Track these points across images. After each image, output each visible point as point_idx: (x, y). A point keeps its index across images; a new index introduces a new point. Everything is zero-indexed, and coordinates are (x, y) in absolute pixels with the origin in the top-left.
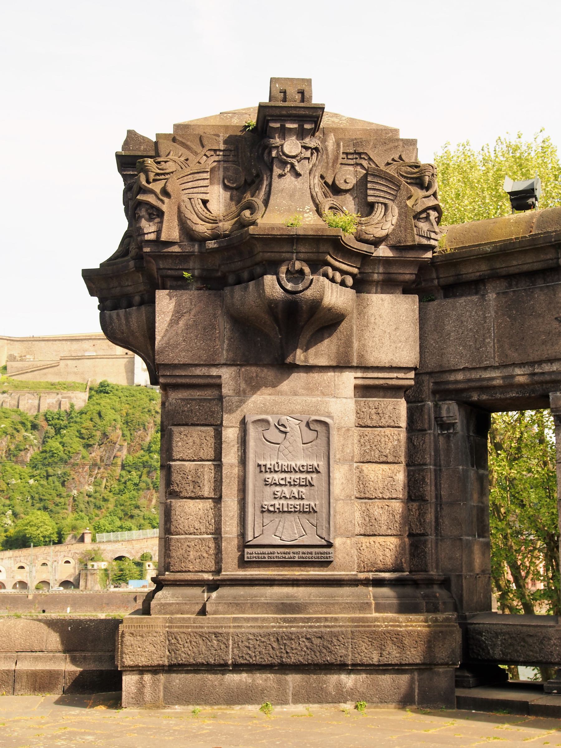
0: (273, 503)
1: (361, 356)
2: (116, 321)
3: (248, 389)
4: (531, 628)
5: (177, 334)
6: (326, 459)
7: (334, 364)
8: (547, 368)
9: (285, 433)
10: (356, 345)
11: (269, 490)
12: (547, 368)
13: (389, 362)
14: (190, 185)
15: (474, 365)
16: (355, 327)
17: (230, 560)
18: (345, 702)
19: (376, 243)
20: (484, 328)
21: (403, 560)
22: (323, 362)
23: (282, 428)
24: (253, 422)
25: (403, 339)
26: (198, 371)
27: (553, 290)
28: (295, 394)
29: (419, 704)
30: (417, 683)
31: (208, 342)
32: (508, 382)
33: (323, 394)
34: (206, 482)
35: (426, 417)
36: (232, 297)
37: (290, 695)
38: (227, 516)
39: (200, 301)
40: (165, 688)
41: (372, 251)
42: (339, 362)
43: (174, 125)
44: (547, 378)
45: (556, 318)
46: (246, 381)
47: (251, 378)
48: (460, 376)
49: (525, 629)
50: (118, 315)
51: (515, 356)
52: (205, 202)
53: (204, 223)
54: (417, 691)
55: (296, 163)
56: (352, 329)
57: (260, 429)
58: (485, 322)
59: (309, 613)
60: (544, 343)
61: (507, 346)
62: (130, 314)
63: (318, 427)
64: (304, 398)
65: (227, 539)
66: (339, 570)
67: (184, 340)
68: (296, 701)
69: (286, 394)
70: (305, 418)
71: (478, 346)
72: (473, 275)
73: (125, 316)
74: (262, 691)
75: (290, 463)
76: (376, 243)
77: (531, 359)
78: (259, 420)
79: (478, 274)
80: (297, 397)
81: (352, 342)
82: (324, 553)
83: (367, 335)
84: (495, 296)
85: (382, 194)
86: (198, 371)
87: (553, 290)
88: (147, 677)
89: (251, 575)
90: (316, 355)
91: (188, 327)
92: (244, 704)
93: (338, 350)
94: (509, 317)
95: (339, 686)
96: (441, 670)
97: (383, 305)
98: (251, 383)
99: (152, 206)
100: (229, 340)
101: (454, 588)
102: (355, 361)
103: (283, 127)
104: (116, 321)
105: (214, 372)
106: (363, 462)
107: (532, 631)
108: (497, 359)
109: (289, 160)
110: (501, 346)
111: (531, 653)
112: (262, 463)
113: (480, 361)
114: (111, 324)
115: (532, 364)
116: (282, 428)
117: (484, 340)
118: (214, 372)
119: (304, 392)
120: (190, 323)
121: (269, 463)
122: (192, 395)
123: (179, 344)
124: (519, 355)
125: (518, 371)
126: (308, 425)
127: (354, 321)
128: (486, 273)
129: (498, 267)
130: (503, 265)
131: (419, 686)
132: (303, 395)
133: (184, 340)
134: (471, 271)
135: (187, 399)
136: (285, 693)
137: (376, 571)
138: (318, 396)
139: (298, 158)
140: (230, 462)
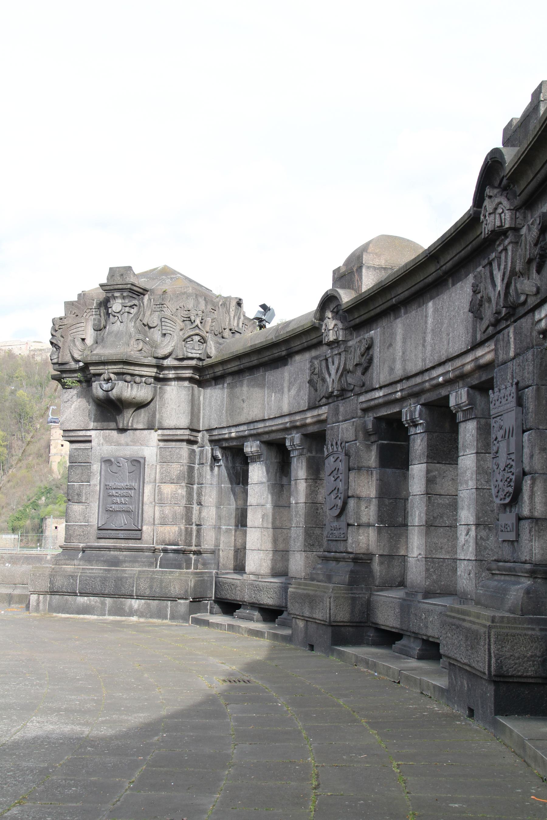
0: (111, 506)
1: (160, 423)
3: (104, 443)
5: (70, 413)
7: (146, 428)
11: (110, 499)
13: (174, 426)
14: (74, 330)
16: (158, 407)
17: (91, 537)
18: (133, 617)
19: (165, 358)
21: (179, 539)
22: (140, 426)
24: (104, 461)
25: (182, 412)
28: (127, 445)
29: (170, 620)
30: (169, 608)
31: (85, 417)
33: (142, 445)
34: (84, 494)
35: (204, 456)
37: (107, 611)
39: (82, 395)
40: (49, 604)
42: (149, 426)
43: (111, 269)
46: (103, 438)
47: (106, 436)
52: (83, 340)
54: (169, 612)
55: (119, 316)
56: (156, 408)
57: (108, 465)
59: (123, 567)
63: (135, 463)
64: (132, 447)
67: (74, 417)
68: (110, 614)
69: (123, 445)
74: (94, 608)
76: (165, 358)
79: (220, 372)
80: (128, 447)
81: (156, 415)
83: (164, 410)
85: (169, 328)
88: (41, 597)
90: (137, 422)
91: (76, 409)
92: (85, 614)
93: (148, 419)
95: (131, 607)
97: (172, 392)
98: (106, 439)
101: (216, 555)
102: (157, 425)
103: (113, 295)
106: (161, 483)
109: (116, 314)
110: (227, 418)
112: (107, 484)
118: (88, 433)
119: (132, 444)
120: (77, 407)
121: (111, 484)
122: (80, 446)
123: (71, 419)
127: (157, 403)
131: (170, 610)
132: (131, 445)
133: (74, 417)
135: (77, 449)
136: (105, 610)
137: (165, 545)
138: (139, 446)
139: (121, 313)
140: (94, 483)
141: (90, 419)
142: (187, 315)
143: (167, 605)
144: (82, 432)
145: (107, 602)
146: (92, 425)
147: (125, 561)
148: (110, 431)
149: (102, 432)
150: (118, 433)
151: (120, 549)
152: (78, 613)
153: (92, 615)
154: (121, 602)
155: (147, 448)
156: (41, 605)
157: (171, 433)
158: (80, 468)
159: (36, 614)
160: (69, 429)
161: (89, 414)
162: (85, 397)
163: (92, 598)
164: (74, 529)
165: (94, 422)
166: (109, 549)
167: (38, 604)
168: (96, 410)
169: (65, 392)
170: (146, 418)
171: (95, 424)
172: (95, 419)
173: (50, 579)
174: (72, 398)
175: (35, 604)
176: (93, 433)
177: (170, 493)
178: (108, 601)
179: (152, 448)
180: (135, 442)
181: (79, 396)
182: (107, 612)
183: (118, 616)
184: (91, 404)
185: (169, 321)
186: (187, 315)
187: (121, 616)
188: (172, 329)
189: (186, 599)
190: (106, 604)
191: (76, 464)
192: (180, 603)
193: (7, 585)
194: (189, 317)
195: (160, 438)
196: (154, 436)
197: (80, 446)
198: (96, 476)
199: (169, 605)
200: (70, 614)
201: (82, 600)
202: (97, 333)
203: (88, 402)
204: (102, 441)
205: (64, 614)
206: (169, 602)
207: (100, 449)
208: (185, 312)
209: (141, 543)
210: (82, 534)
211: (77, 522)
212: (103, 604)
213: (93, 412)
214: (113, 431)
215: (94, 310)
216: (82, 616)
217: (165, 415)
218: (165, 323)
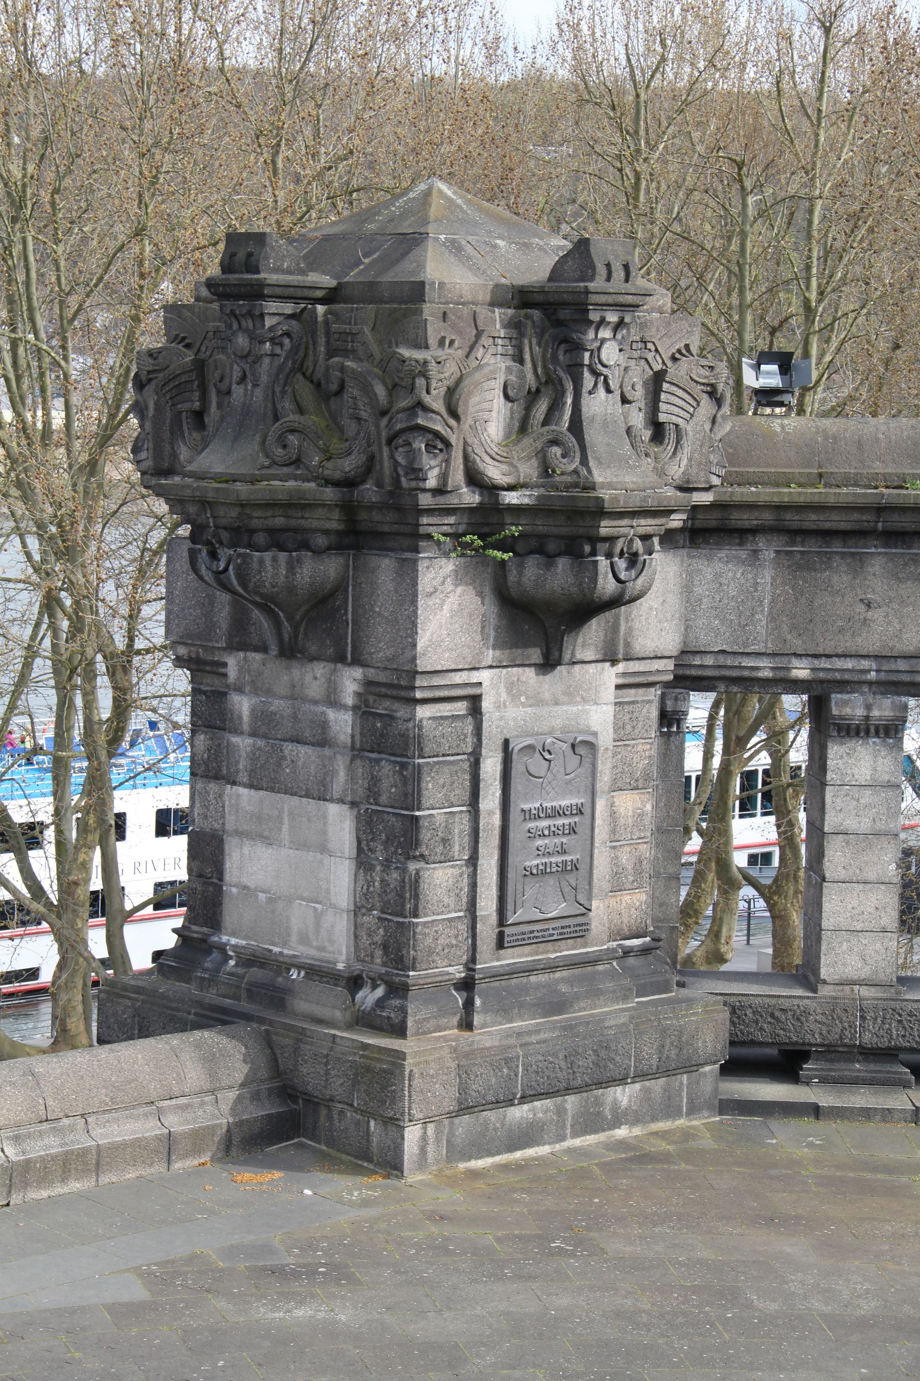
1: (627, 645)
2: (269, 568)
4: (782, 1000)
5: (441, 626)
6: (590, 794)
8: (839, 664)
9: (550, 761)
10: (623, 628)
12: (839, 664)
15: (736, 648)
20: (753, 598)
23: (547, 756)
26: (458, 678)
27: (861, 560)
28: (557, 703)
32: (781, 674)
36: (520, 574)
38: (483, 885)
40: (448, 1142)
41: (433, 392)
44: (838, 676)
45: (861, 600)
48: (709, 661)
49: (773, 1001)
50: (275, 560)
51: (798, 645)
53: (496, 464)
58: (756, 590)
60: (841, 630)
61: (785, 628)
62: (299, 561)
63: (581, 750)
65: (484, 917)
66: (593, 946)
68: (575, 1135)
69: (548, 704)
70: (570, 738)
71: (743, 622)
72: (747, 523)
73: (287, 563)
75: (554, 804)
77: (820, 650)
78: (525, 747)
79: (755, 522)
82: (580, 925)
84: (773, 555)
85: (676, 410)
86: (458, 678)
87: (861, 560)
89: (508, 965)
91: (454, 614)
94: (793, 588)
96: (707, 1068)
99: (437, 435)
100: (496, 631)
104: (269, 568)
105: (475, 677)
107: (785, 1004)
108: (770, 645)
111: (782, 1032)
113: (746, 644)
114: (260, 572)
115: (816, 656)
116: (547, 756)
117: (753, 615)
118: (475, 677)
119: (566, 699)
120: (455, 607)
122: (440, 711)
124: (804, 642)
125: (795, 662)
126: (573, 746)
128: (767, 523)
129: (788, 518)
130: (797, 518)
132: (564, 704)
134: (746, 517)
141: (485, 638)
142: (706, 377)
143: (681, 1083)
144: (460, 673)
145: (568, 1106)
146: (490, 656)
147: (577, 997)
148: (520, 669)
149: (504, 671)
150: (537, 675)
151: (551, 967)
152: (511, 1149)
153: (538, 1145)
154: (596, 1098)
155: (594, 707)
156: (430, 1149)
157: (642, 669)
158: (446, 769)
159: (419, 1177)
160: (439, 668)
161: (483, 628)
162: (472, 583)
163: (537, 1104)
164: (436, 932)
165: (494, 648)
166: (529, 970)
167: (423, 1150)
168: (499, 616)
169: (428, 568)
170: (601, 634)
171: (498, 653)
172: (496, 639)
173: (460, 1077)
174: (443, 583)
175: (416, 1150)
176: (484, 676)
177: (630, 813)
178: (571, 1102)
179: (605, 707)
180: (571, 695)
181: (459, 578)
182: (568, 1131)
183: (590, 1133)
184: (487, 601)
185: (680, 393)
186: (706, 377)
187: (596, 1132)
188: (682, 413)
189: (715, 1063)
190: (565, 1110)
191: (435, 759)
192: (705, 1074)
193: (135, 1112)
194: (712, 385)
195: (621, 681)
196: (610, 675)
197: (440, 711)
198: (492, 789)
199: (685, 1082)
200: (493, 1155)
201: (519, 1113)
202: (511, 409)
203: (480, 594)
204: (504, 696)
205: (481, 1158)
206: (685, 1076)
207: (501, 718)
208: (702, 371)
209: (585, 945)
210: (454, 942)
211: (442, 913)
212: (560, 1111)
213: (493, 620)
214: (527, 669)
215: (500, 341)
216: (518, 1154)
217: (637, 625)
218: (669, 396)
